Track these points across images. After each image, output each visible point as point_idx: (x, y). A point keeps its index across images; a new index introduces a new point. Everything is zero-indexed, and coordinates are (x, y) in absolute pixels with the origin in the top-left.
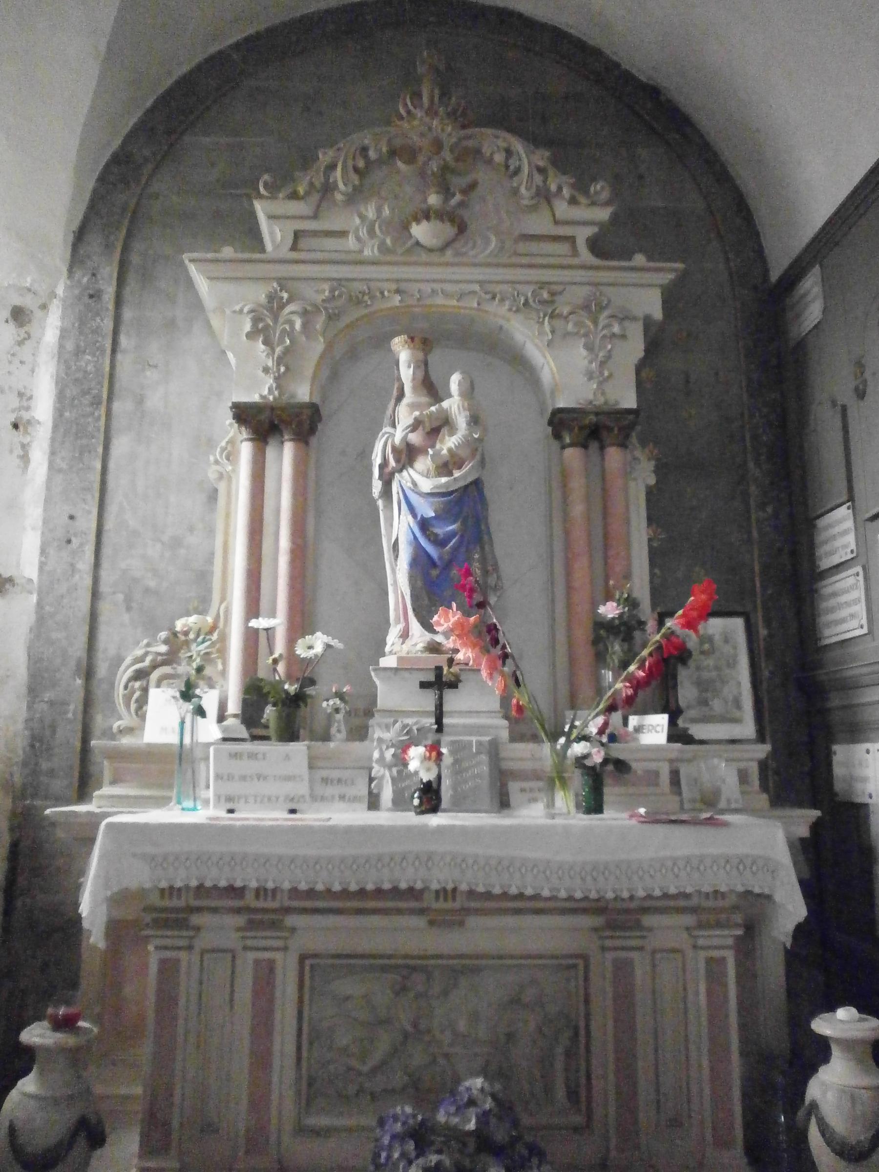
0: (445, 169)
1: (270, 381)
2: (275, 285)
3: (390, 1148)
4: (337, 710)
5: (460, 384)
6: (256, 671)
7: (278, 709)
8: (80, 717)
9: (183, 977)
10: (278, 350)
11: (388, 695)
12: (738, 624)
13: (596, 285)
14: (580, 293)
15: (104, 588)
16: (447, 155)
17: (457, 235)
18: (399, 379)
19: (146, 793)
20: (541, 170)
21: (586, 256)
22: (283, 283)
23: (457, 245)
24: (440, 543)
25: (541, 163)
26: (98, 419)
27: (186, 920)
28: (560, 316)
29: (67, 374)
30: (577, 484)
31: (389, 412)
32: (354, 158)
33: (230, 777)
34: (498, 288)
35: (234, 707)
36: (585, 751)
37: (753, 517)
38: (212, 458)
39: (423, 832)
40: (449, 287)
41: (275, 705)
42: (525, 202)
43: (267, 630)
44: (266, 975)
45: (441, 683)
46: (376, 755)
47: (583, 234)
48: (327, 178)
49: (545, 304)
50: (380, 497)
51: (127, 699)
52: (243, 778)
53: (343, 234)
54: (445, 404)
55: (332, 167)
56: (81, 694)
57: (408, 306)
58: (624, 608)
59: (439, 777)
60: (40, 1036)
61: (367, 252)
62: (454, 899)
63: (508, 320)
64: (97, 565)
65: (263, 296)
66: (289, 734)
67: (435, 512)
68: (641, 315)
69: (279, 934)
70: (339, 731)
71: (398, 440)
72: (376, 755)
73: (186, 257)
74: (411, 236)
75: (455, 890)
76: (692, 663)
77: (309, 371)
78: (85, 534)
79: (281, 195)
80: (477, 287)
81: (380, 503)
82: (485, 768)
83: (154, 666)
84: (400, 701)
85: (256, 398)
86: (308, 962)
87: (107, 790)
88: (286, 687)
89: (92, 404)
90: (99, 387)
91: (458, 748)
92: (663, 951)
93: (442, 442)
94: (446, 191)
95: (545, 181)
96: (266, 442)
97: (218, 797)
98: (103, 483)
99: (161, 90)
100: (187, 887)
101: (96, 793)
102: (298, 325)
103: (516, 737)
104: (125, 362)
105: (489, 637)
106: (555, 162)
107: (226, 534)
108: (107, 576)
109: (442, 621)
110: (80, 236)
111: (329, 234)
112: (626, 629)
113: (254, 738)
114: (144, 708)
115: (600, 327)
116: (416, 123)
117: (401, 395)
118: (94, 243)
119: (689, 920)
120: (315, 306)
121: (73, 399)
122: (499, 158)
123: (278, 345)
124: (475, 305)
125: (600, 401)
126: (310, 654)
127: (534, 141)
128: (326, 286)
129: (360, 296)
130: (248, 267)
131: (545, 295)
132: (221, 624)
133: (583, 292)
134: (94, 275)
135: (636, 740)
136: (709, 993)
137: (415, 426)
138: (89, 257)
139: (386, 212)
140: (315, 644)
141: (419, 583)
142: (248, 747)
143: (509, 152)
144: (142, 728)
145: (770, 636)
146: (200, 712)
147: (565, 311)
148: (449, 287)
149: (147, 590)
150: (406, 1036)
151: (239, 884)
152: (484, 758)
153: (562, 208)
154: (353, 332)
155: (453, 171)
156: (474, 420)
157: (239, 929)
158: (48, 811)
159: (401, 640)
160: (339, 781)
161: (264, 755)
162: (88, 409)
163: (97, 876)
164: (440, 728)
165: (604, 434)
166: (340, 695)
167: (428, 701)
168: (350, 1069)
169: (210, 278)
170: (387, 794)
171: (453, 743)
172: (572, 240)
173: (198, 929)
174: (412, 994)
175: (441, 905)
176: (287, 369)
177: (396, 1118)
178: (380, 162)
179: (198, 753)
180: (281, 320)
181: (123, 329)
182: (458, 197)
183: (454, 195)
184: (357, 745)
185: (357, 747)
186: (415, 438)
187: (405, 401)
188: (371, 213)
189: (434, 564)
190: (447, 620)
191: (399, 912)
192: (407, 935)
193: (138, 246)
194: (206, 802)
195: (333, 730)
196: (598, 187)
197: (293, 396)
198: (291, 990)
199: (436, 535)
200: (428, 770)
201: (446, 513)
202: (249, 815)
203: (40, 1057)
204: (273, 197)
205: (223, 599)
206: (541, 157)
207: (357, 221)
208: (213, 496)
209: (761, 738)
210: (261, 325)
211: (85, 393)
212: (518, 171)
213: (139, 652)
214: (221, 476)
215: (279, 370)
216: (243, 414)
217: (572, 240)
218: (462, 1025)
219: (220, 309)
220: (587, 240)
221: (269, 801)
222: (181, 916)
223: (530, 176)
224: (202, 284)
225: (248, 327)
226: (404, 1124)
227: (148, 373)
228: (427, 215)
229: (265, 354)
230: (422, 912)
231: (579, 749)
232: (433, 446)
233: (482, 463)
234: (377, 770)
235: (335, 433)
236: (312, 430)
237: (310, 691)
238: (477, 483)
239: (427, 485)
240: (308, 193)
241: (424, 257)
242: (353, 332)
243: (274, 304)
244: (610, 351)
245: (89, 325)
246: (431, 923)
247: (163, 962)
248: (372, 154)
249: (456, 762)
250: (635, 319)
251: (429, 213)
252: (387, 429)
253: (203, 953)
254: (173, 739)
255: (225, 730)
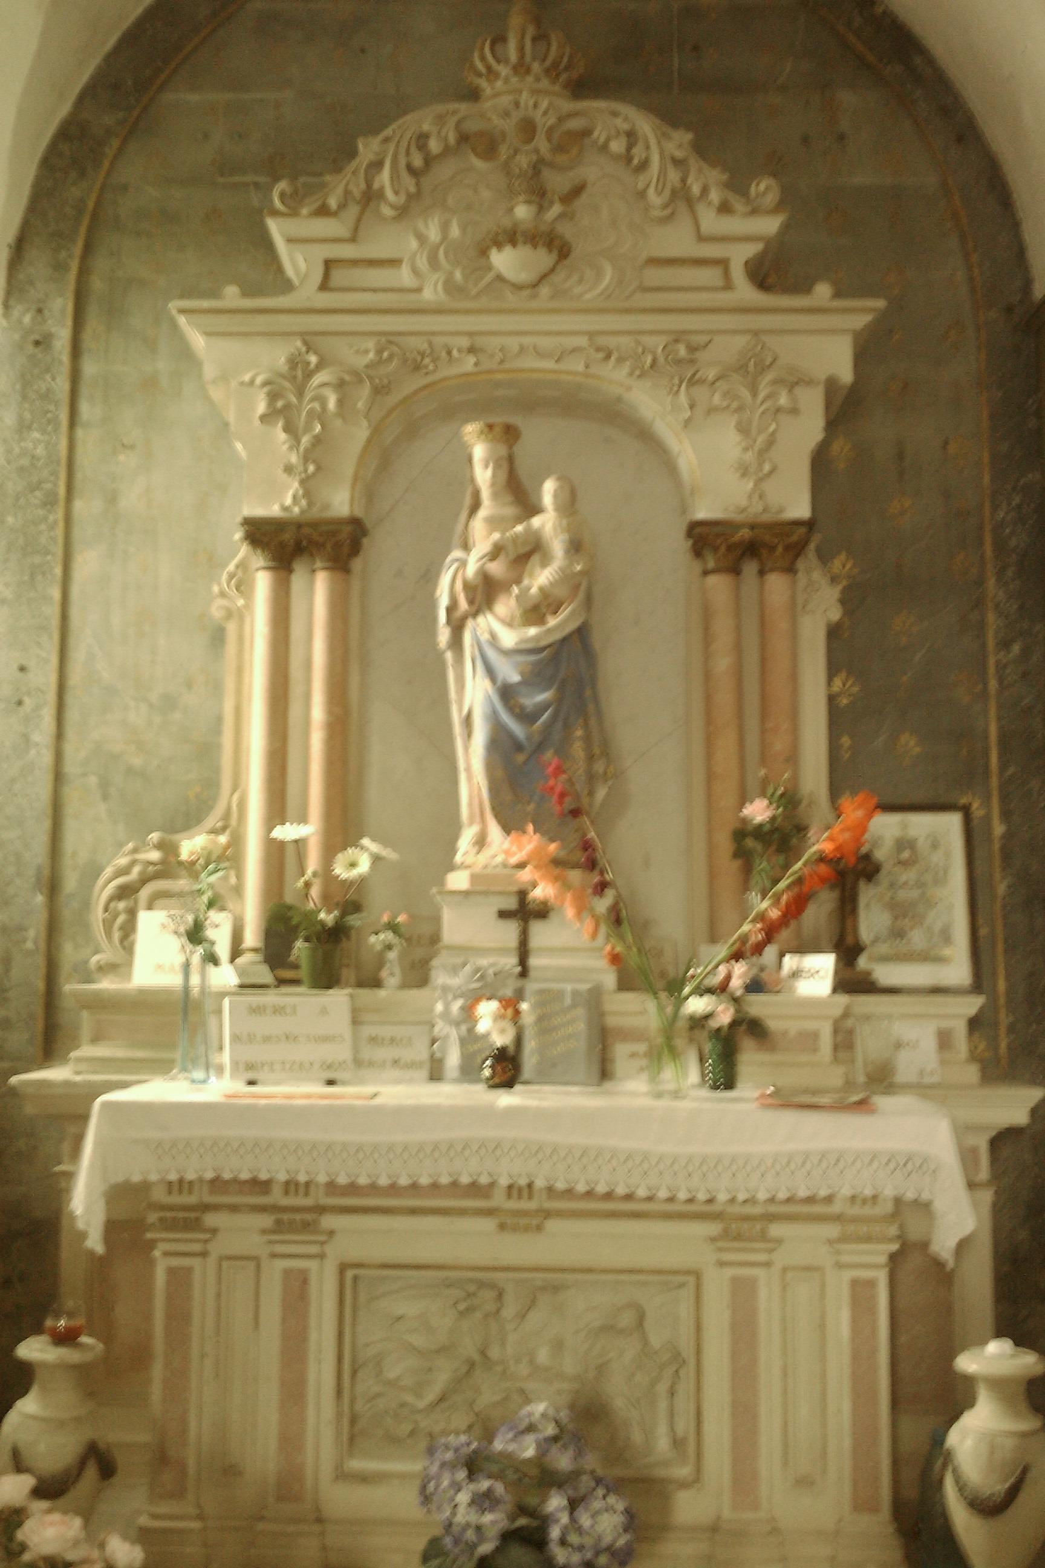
0: (536, 170)
1: (293, 487)
2: (299, 343)
3: (438, 1477)
4: (389, 947)
5: (556, 496)
6: (281, 894)
7: (314, 945)
8: (42, 945)
9: (196, 1292)
10: (305, 440)
11: (456, 926)
12: (951, 824)
13: (756, 333)
14: (731, 346)
15: (71, 768)
16: (542, 144)
17: (557, 263)
18: (472, 480)
19: (140, 1054)
20: (677, 163)
21: (745, 291)
22: (310, 341)
23: (557, 278)
24: (527, 717)
25: (679, 154)
26: (52, 527)
27: (197, 1220)
28: (702, 381)
29: (9, 463)
30: (723, 626)
31: (460, 527)
32: (408, 153)
33: (251, 1038)
34: (611, 342)
35: (252, 937)
36: (709, 1009)
37: (991, 661)
38: (216, 589)
39: (489, 1113)
40: (545, 342)
41: (307, 940)
42: (656, 213)
43: (296, 841)
44: (297, 1291)
45: (525, 912)
46: (439, 1007)
47: (740, 255)
48: (369, 185)
49: (680, 364)
50: (443, 653)
51: (108, 925)
52: (267, 1039)
53: (394, 263)
54: (536, 521)
55: (378, 165)
56: (42, 916)
57: (488, 372)
58: (778, 807)
59: (519, 1040)
60: (41, 1351)
61: (428, 295)
62: (530, 1197)
63: (629, 389)
64: (60, 735)
65: (283, 359)
66: (326, 978)
67: (522, 674)
68: (823, 377)
69: (312, 1238)
70: (392, 974)
71: (471, 570)
72: (439, 1007)
73: (173, 305)
74: (489, 268)
75: (530, 1186)
76: (883, 876)
77: (348, 469)
78: (42, 692)
79: (305, 211)
80: (583, 341)
81: (449, 656)
82: (581, 1026)
83: (144, 880)
84: (473, 932)
85: (274, 510)
86: (350, 1274)
87: (86, 1050)
88: (322, 915)
89: (44, 504)
90: (52, 478)
91: (547, 1000)
92: (794, 1268)
93: (531, 575)
94: (539, 196)
95: (684, 180)
96: (290, 571)
97: (235, 1064)
98: (64, 617)
99: (126, 24)
100: (201, 1180)
101: (73, 1055)
102: (332, 404)
103: (625, 984)
104: (88, 441)
105: (586, 861)
106: (700, 149)
107: (239, 692)
108: (75, 753)
109: (514, 849)
110: (19, 248)
111: (372, 263)
112: (783, 837)
113: (281, 982)
114: (131, 938)
115: (762, 395)
116: (499, 84)
117: (475, 506)
118: (38, 263)
119: (832, 1230)
120: (356, 374)
121: (17, 499)
122: (617, 146)
123: (304, 434)
124: (581, 368)
125: (757, 507)
126: (355, 873)
127: (670, 118)
128: (370, 344)
129: (419, 359)
130: (261, 319)
131: (682, 351)
132: (234, 822)
133: (740, 342)
134: (40, 311)
135: (792, 990)
136: (855, 1321)
137: (496, 552)
138: (31, 283)
139: (455, 231)
140: (357, 863)
141: (500, 773)
142: (271, 998)
143: (631, 136)
144: (129, 963)
145: (1008, 836)
146: (212, 959)
147: (711, 374)
148: (545, 342)
149: (130, 771)
150: (472, 1365)
151: (263, 1176)
152: (580, 1012)
153: (710, 221)
154: (408, 401)
155: (551, 165)
156: (575, 547)
157: (264, 1232)
158: (14, 1080)
159: (477, 848)
160: (392, 1040)
161: (294, 1007)
162: (41, 512)
163: (92, 1165)
164: (524, 974)
165: (764, 552)
166: (393, 927)
167: (510, 932)
168: (403, 1405)
169: (208, 334)
170: (453, 1059)
171: (542, 992)
172: (723, 263)
173: (214, 1231)
174: (478, 1315)
175: (513, 1204)
176: (319, 468)
177: (447, 1447)
178: (447, 151)
179: (209, 1005)
180: (308, 396)
181: (84, 390)
182: (556, 209)
183: (552, 203)
184: (414, 993)
185: (414, 995)
186: (496, 568)
187: (482, 513)
188: (433, 233)
189: (518, 747)
190: (520, 848)
191: (462, 1212)
192: (470, 1242)
193: (101, 264)
194: (220, 1070)
195: (384, 974)
196: (762, 187)
197: (327, 507)
198: (329, 1305)
199: (522, 708)
200: (502, 1031)
201: (536, 677)
202: (278, 1090)
203: (40, 1375)
204: (294, 213)
205: (235, 787)
206: (680, 141)
207: (414, 244)
208: (218, 637)
209: (978, 985)
210: (280, 404)
211: (33, 488)
212: (644, 165)
213: (123, 861)
214: (229, 614)
215: (306, 470)
216: (259, 533)
217: (723, 263)
218: (543, 1356)
219: (223, 378)
220: (746, 263)
221: (298, 1070)
222: (192, 1215)
223: (663, 172)
224: (198, 341)
225: (261, 407)
226: (456, 1450)
227: (122, 458)
228: (511, 237)
229: (286, 446)
230: (489, 1212)
231: (697, 1005)
232: (518, 581)
233: (589, 602)
234: (441, 1028)
235: (384, 552)
236: (355, 548)
237: (353, 920)
238: (582, 633)
239: (509, 638)
240: (342, 206)
241: (511, 299)
242: (408, 401)
243: (298, 373)
244: (773, 434)
245: (35, 387)
246: (502, 1227)
247: (171, 1272)
248: (434, 146)
249: (540, 1019)
250: (810, 382)
251: (515, 233)
252: (457, 553)
253: (221, 1259)
254: (173, 980)
255: (241, 972)
